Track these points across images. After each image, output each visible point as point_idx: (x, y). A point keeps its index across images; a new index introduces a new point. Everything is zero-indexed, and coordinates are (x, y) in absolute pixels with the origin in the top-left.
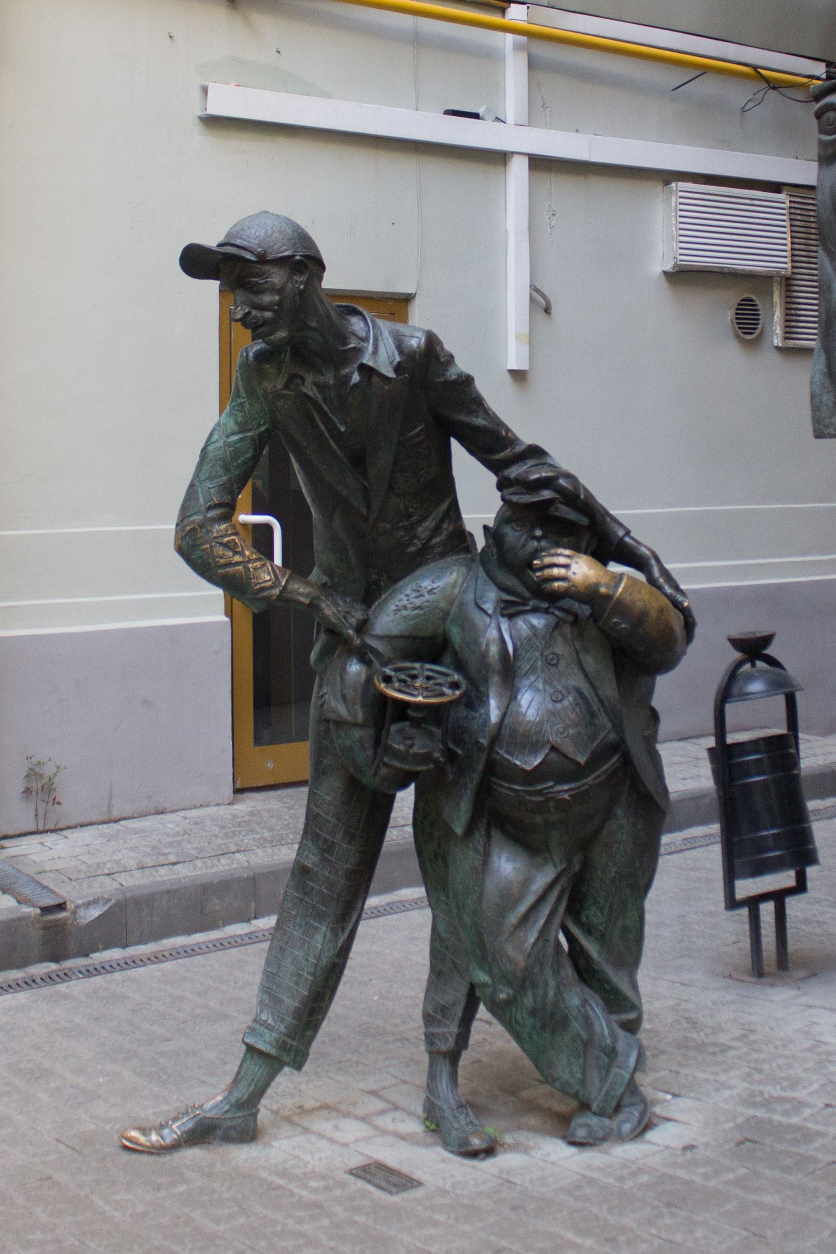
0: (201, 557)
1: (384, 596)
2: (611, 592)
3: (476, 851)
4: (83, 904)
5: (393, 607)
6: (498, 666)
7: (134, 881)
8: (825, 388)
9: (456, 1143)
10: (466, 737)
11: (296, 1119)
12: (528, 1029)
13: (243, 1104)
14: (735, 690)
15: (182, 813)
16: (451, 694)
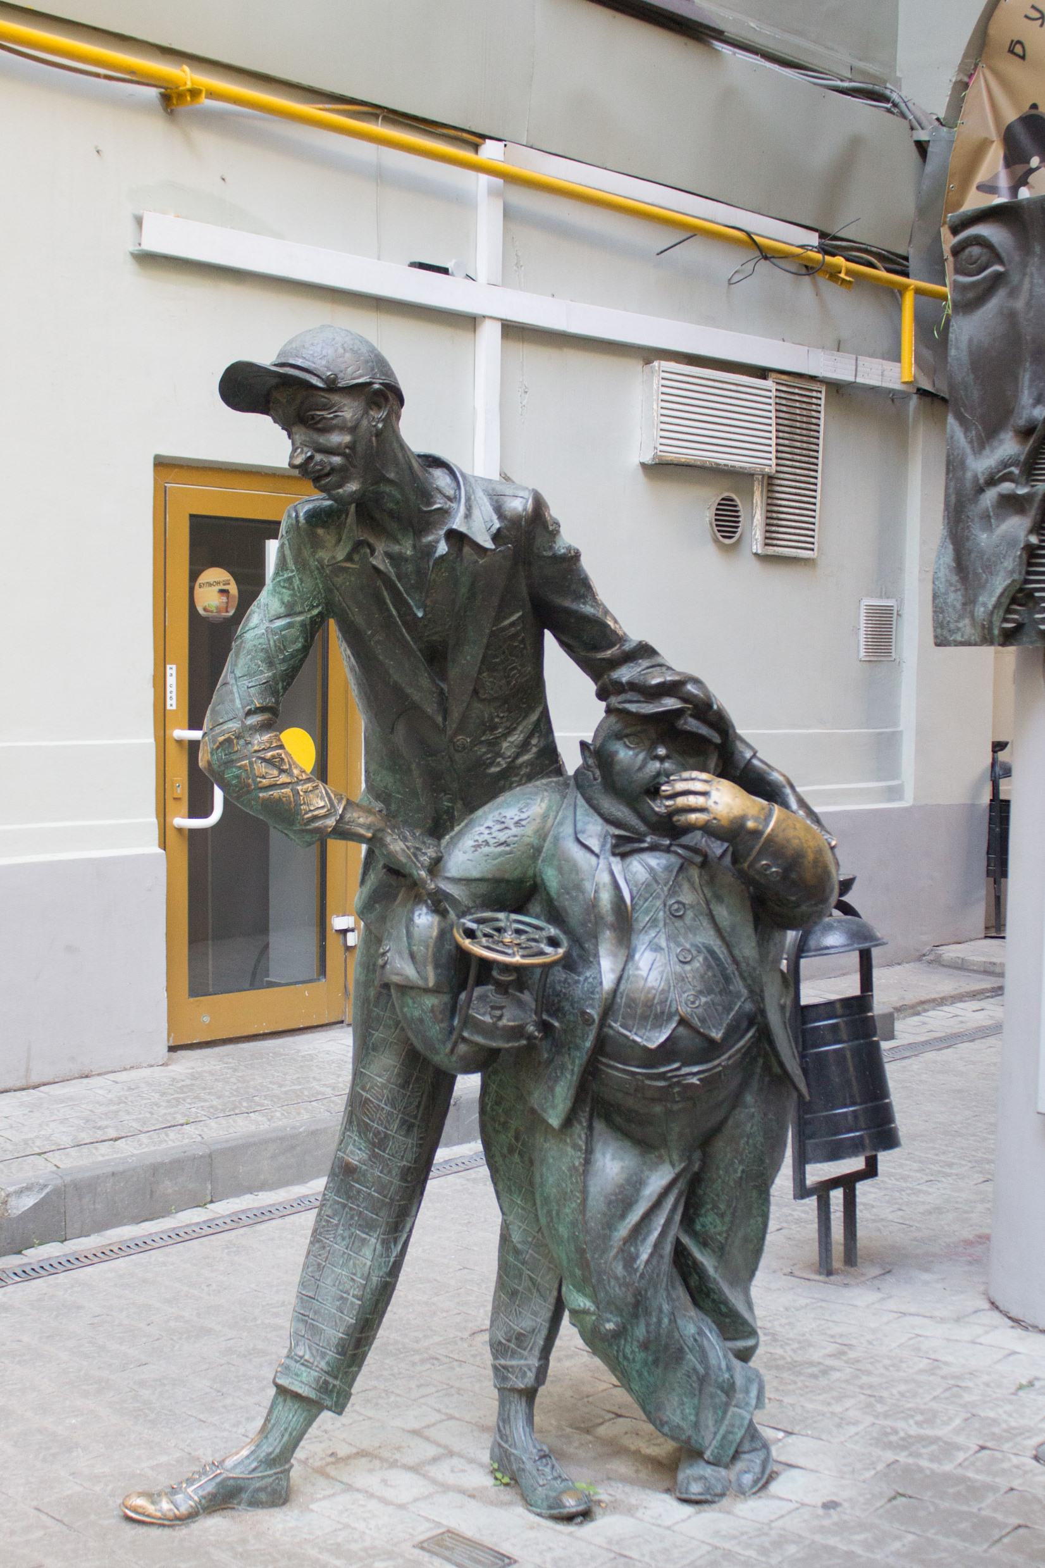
0: (238, 777)
1: (457, 829)
2: (761, 827)
3: (575, 1147)
4: (15, 1192)
5: (471, 843)
6: (610, 919)
7: (75, 1163)
8: (951, 585)
9: (545, 1504)
10: (567, 1006)
11: (331, 1471)
12: (638, 1366)
13: (274, 1460)
14: (812, 943)
15: (111, 1076)
16: (553, 954)
